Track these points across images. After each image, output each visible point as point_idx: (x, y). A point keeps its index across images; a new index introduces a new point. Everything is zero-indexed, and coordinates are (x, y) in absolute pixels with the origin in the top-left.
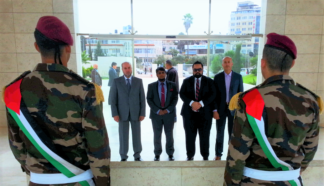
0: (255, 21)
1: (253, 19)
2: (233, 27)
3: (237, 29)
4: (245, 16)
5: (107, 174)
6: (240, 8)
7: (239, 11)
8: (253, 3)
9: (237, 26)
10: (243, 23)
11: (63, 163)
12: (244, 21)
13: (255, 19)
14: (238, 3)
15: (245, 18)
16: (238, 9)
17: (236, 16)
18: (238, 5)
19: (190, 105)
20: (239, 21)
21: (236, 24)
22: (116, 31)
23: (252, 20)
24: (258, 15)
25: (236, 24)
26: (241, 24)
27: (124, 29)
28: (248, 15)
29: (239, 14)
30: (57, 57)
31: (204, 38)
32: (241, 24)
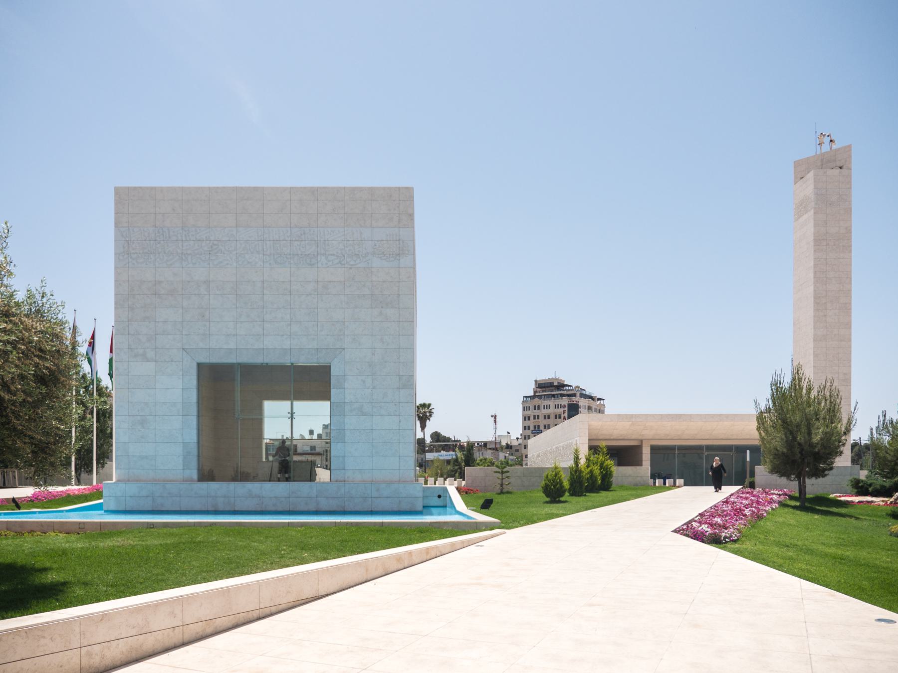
0: (567, 412)
1: (562, 410)
2: (528, 423)
3: (535, 427)
4: (548, 404)
5: (873, 492)
6: (538, 389)
7: (537, 394)
8: (564, 381)
9: (535, 420)
10: (545, 416)
11: (40, 512)
12: (546, 412)
13: (566, 409)
14: (536, 381)
15: (548, 407)
16: (535, 392)
17: (530, 404)
18: (536, 384)
19: (716, 458)
20: (537, 412)
21: (532, 418)
22: (283, 436)
23: (561, 410)
24: (570, 403)
25: (540, 418)
26: (541, 417)
27: (324, 428)
28: (551, 402)
29: (537, 401)
30: (843, 511)
31: (48, 511)
32: (541, 417)
